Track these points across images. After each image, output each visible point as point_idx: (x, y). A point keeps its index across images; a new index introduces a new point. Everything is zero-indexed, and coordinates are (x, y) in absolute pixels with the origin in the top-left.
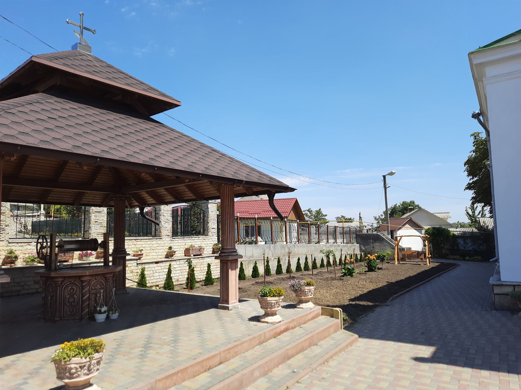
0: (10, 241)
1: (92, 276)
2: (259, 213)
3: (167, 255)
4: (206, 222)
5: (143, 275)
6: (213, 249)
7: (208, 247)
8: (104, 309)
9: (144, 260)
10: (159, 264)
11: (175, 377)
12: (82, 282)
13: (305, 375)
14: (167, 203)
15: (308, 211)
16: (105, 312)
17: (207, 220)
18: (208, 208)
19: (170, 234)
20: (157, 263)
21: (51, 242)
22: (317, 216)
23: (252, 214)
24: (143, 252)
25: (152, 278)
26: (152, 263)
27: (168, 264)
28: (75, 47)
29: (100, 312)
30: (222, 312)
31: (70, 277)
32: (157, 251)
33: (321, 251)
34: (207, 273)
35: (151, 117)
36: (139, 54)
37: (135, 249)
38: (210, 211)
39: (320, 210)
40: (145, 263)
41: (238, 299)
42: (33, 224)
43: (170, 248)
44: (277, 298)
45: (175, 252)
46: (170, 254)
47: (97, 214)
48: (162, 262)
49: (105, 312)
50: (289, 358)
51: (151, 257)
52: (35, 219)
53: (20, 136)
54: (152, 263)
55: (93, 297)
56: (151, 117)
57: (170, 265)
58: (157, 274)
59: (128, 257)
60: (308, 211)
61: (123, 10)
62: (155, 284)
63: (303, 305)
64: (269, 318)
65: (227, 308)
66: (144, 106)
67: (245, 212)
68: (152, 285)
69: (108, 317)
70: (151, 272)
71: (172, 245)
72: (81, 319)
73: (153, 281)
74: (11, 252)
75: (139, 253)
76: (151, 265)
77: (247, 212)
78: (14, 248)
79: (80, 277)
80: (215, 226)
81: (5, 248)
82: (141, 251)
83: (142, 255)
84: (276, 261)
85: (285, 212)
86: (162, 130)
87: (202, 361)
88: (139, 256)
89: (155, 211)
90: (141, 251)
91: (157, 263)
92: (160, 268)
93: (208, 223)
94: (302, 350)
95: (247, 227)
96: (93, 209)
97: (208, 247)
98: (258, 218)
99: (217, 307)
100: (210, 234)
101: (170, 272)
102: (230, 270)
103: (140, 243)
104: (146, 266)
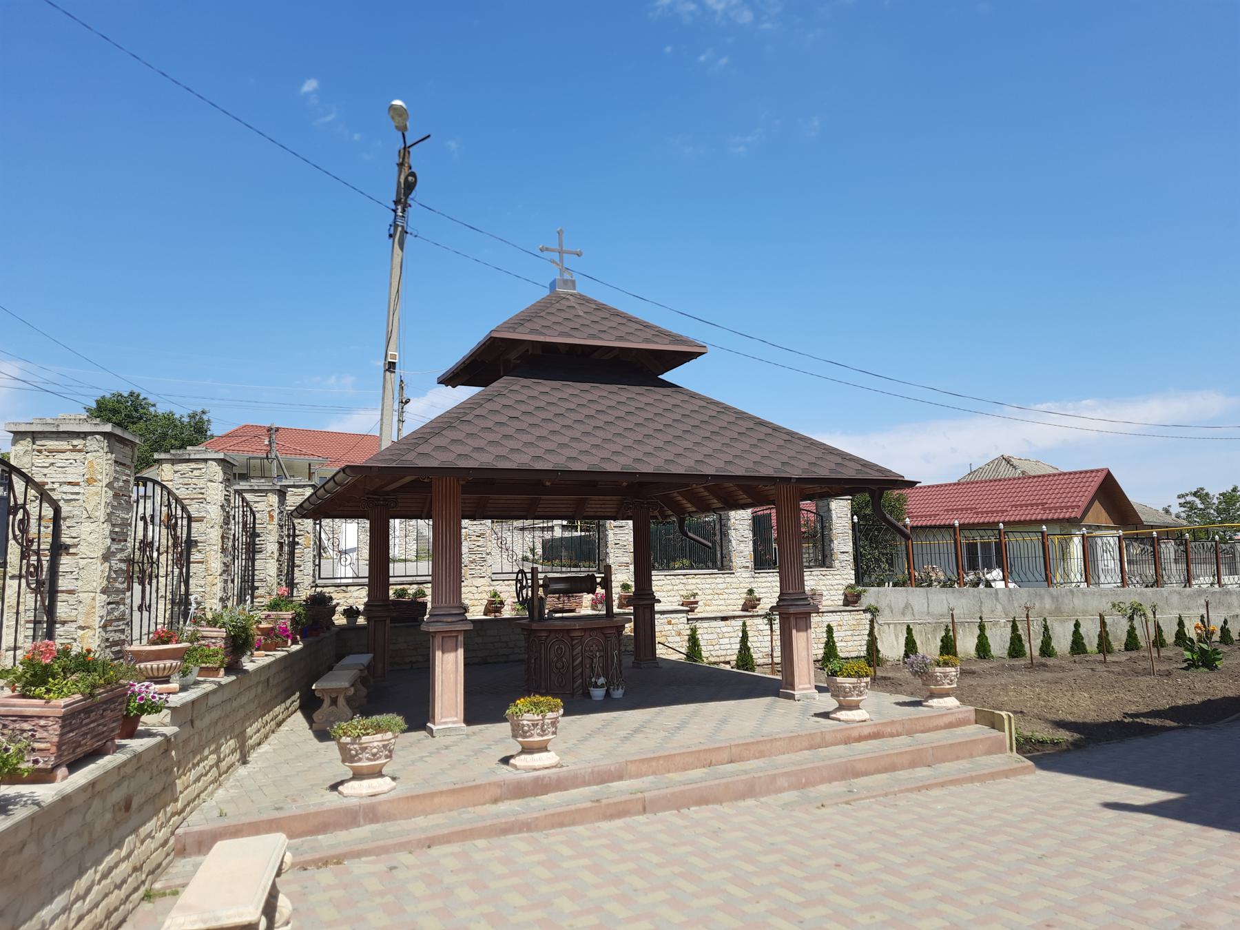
0: (494, 577)
1: (584, 630)
2: (935, 515)
3: (745, 604)
4: (827, 540)
5: (693, 640)
6: (846, 596)
7: (833, 593)
8: (601, 681)
9: (700, 612)
10: (728, 622)
11: (654, 764)
12: (572, 639)
13: (867, 798)
14: (744, 507)
15: (1195, 494)
16: (602, 686)
17: (829, 535)
18: (829, 510)
19: (751, 565)
20: (724, 619)
21: (532, 579)
22: (1226, 510)
23: (982, 513)
24: (697, 598)
25: (717, 647)
26: (715, 619)
27: (739, 622)
28: (553, 285)
29: (596, 686)
30: (782, 702)
31: (556, 631)
32: (726, 596)
33: (1114, 606)
34: (827, 644)
35: (664, 377)
36: (741, 149)
37: (684, 593)
38: (834, 516)
39: (1235, 490)
40: (702, 619)
41: (813, 684)
42: (545, 544)
43: (751, 592)
44: (854, 680)
45: (759, 600)
46: (751, 604)
47: (617, 531)
48: (734, 617)
49: (602, 686)
50: (857, 775)
51: (715, 608)
52: (548, 535)
53: (475, 455)
54: (715, 619)
55: (588, 661)
56: (664, 377)
57: (744, 624)
58: (727, 641)
59: (658, 607)
60: (1195, 494)
61: (702, 58)
62: (722, 659)
63: (934, 702)
64: (843, 712)
65: (791, 697)
66: (643, 366)
67: (967, 509)
68: (717, 660)
69: (608, 694)
70: (715, 636)
71: (754, 585)
72: (573, 694)
73: (719, 653)
74: (495, 595)
75: (692, 599)
76: (714, 624)
77: (971, 509)
78: (498, 589)
79: (568, 631)
80: (849, 547)
81: (487, 589)
82: (694, 595)
83: (696, 603)
84: (1010, 625)
85: (1073, 507)
86: (677, 399)
87: (699, 751)
88: (690, 605)
89: (721, 520)
90: (694, 595)
91: (724, 619)
92: (730, 629)
93: (831, 541)
94: (892, 768)
95: (972, 548)
96: (610, 524)
97: (833, 593)
98: (963, 527)
99: (777, 694)
100: (837, 564)
101: (745, 633)
102: (794, 632)
103: (694, 581)
104: (698, 624)
